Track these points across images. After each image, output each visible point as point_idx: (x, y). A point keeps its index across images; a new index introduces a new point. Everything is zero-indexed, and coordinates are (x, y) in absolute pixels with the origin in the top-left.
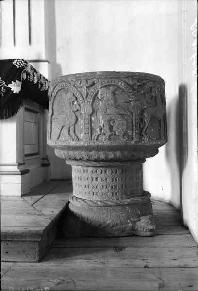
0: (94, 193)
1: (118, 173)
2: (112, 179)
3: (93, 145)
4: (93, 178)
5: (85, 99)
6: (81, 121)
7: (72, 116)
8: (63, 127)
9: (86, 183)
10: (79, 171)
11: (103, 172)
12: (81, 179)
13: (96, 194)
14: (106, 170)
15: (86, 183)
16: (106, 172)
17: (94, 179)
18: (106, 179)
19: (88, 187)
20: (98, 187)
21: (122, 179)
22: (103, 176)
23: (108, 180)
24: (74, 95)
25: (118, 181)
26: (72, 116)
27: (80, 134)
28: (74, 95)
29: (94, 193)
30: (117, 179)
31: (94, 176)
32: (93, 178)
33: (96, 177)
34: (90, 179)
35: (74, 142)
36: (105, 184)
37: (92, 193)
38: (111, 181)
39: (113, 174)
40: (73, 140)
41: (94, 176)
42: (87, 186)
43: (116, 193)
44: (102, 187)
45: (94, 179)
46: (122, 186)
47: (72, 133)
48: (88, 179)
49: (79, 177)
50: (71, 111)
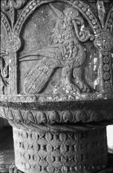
0: (41, 167)
1: (75, 138)
2: (68, 147)
3: (18, 101)
4: (39, 146)
5: (102, 23)
6: (93, 58)
7: (78, 50)
8: (55, 70)
9: (30, 152)
10: (21, 135)
11: (55, 137)
12: (23, 146)
13: (45, 169)
14: (59, 135)
15: (30, 152)
16: (58, 137)
17: (42, 148)
18: (59, 148)
19: (33, 159)
20: (47, 159)
21: (81, 147)
22: (54, 143)
23: (61, 148)
24: (81, 14)
25: (75, 150)
26: (78, 50)
27: (93, 81)
28: (81, 14)
29: (41, 167)
30: (75, 146)
31: (42, 143)
32: (39, 146)
33: (44, 144)
34: (36, 147)
35: (84, 96)
36: (57, 155)
37: (39, 167)
38: (66, 150)
39: (68, 140)
40: (81, 92)
41: (42, 143)
42: (31, 157)
43: (73, 168)
44: (53, 159)
45: (42, 148)
46: (82, 156)
47: (78, 81)
48: (32, 147)
49: (20, 143)
50: (76, 42)
